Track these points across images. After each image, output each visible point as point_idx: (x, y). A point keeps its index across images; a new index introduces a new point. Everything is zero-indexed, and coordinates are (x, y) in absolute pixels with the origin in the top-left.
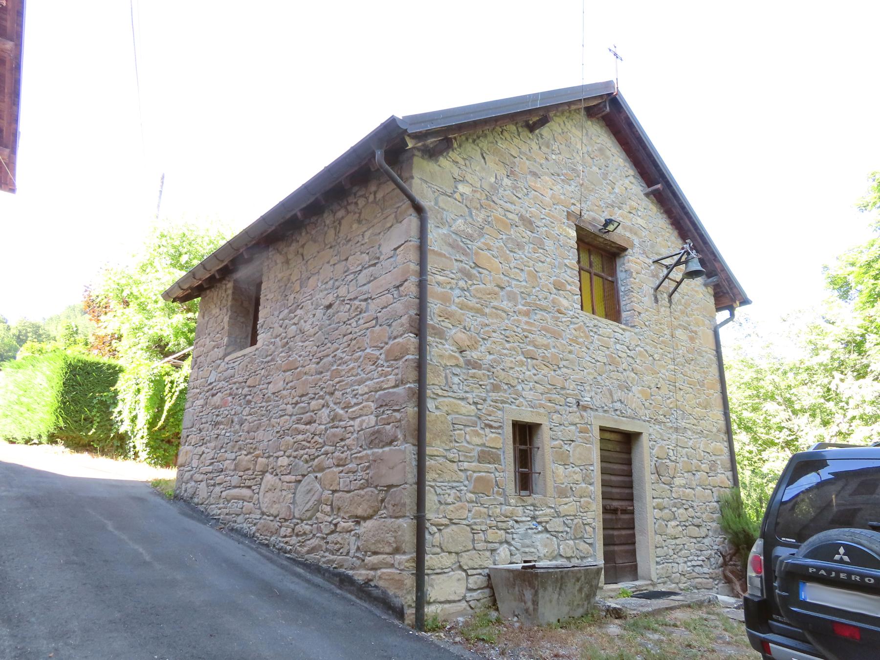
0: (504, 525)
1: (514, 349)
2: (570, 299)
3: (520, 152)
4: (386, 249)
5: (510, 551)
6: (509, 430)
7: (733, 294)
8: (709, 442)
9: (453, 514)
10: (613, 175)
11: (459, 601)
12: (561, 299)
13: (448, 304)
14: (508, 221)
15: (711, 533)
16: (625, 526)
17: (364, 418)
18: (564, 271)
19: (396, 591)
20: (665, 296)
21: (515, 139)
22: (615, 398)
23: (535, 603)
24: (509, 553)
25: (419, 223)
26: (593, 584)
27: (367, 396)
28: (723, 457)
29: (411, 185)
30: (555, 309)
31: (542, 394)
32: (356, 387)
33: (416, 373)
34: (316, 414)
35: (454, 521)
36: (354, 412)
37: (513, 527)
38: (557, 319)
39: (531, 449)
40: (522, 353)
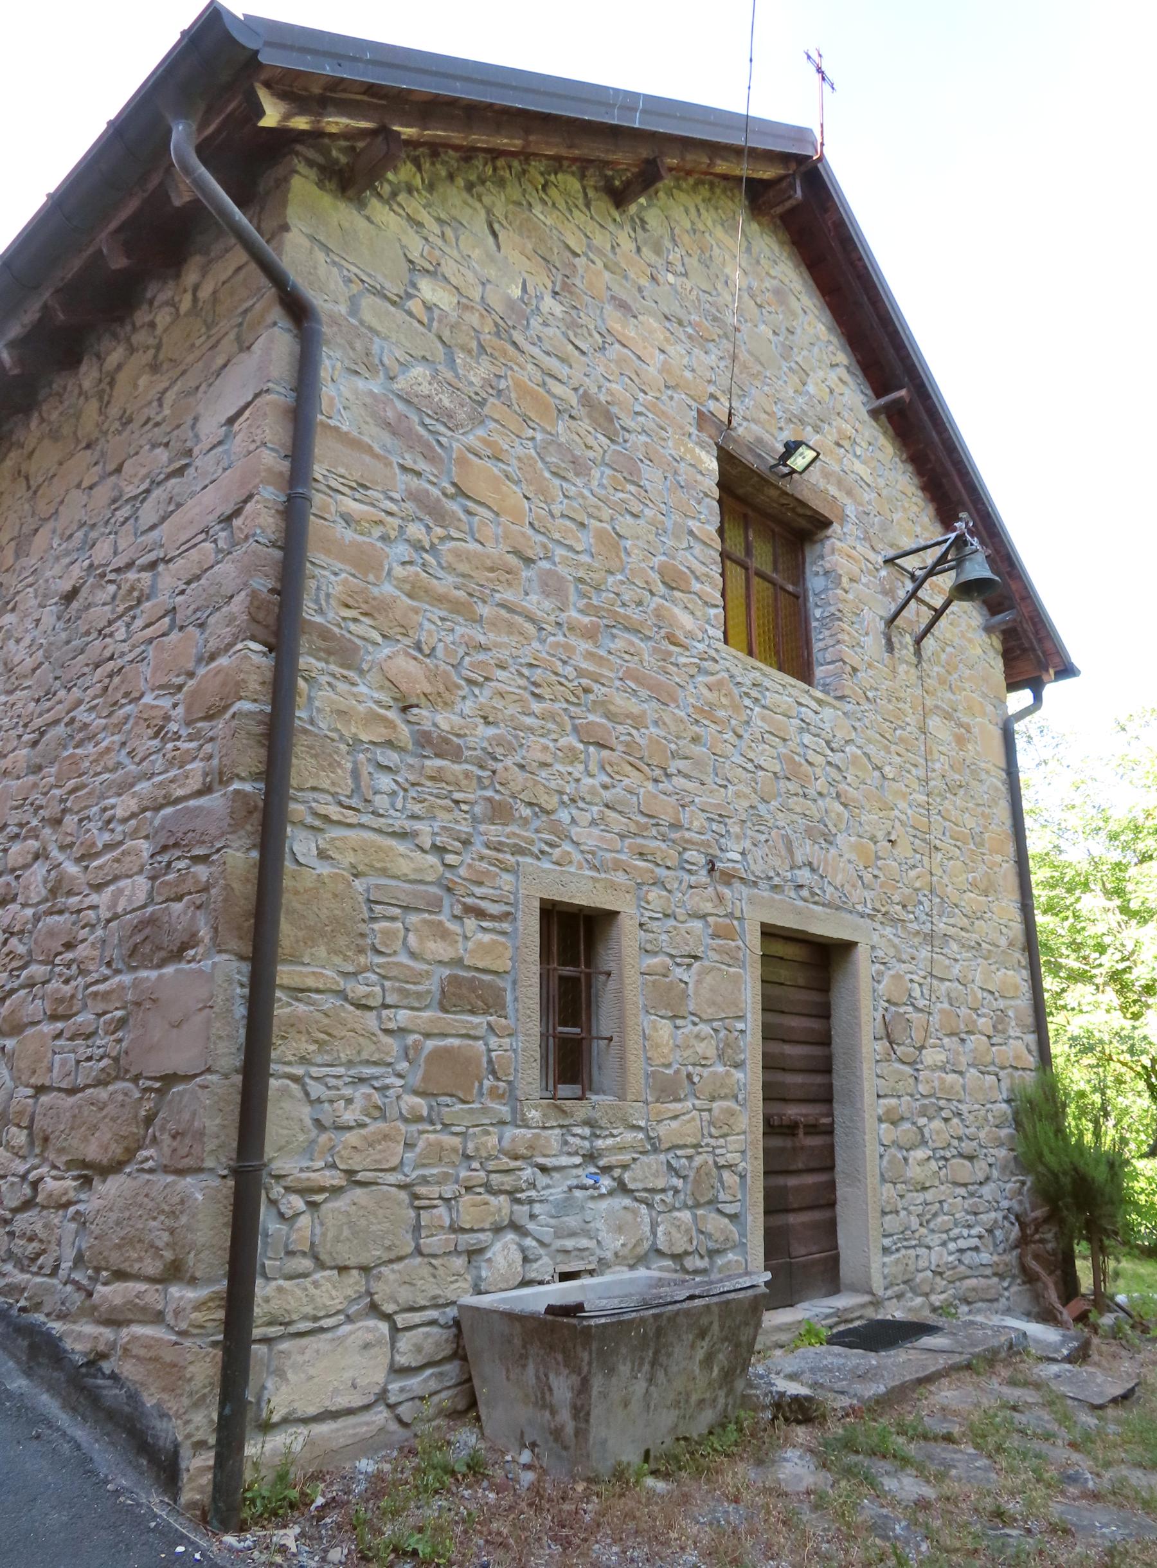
0: (508, 1181)
1: (552, 716)
2: (699, 614)
3: (589, 247)
4: (210, 427)
5: (523, 1250)
6: (530, 925)
7: (1044, 652)
8: (993, 967)
9: (357, 1158)
10: (805, 353)
11: (367, 1407)
12: (677, 611)
13: (371, 578)
14: (552, 400)
15: (995, 1174)
16: (812, 1164)
17: (122, 884)
18: (685, 545)
19: (165, 1397)
20: (908, 639)
21: (576, 212)
22: (799, 859)
23: (581, 1412)
24: (518, 1257)
25: (298, 348)
26: (743, 1339)
27: (133, 822)
28: (1019, 1002)
29: (279, 250)
30: (663, 632)
31: (622, 836)
32: (112, 801)
33: (263, 752)
34: (18, 877)
35: (359, 1177)
36: (100, 867)
37: (533, 1185)
38: (665, 657)
39: (589, 976)
40: (575, 729)
